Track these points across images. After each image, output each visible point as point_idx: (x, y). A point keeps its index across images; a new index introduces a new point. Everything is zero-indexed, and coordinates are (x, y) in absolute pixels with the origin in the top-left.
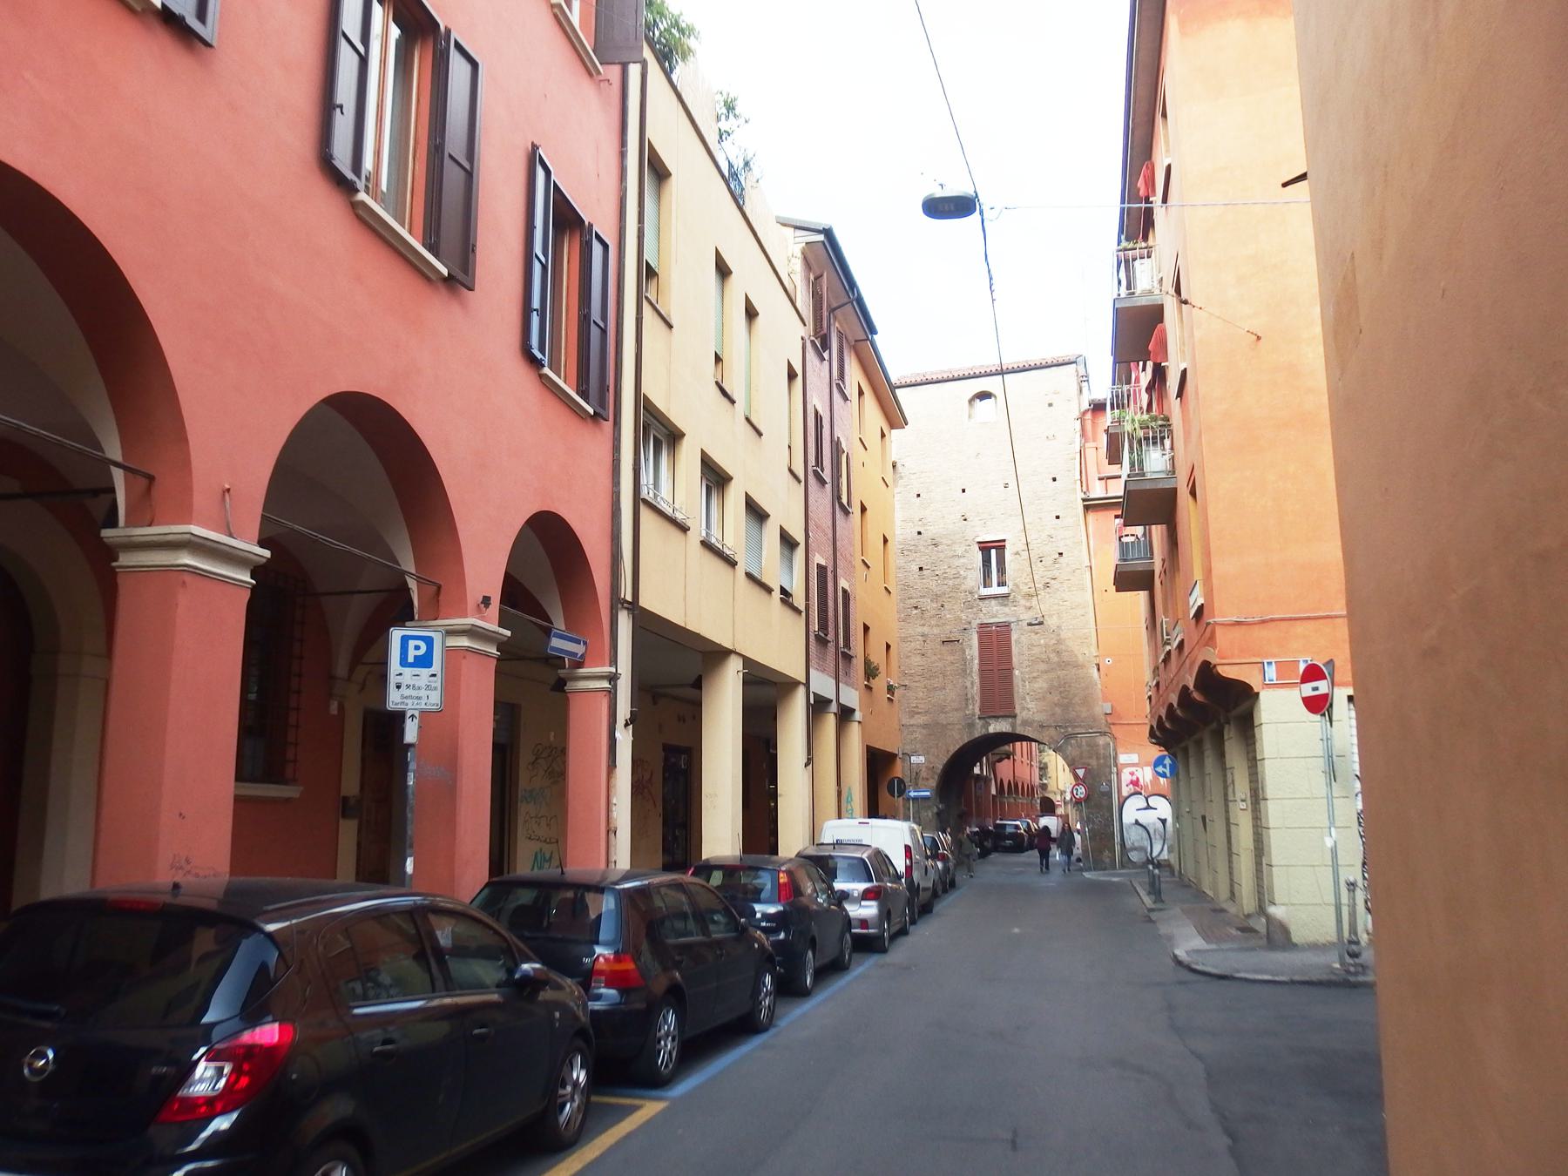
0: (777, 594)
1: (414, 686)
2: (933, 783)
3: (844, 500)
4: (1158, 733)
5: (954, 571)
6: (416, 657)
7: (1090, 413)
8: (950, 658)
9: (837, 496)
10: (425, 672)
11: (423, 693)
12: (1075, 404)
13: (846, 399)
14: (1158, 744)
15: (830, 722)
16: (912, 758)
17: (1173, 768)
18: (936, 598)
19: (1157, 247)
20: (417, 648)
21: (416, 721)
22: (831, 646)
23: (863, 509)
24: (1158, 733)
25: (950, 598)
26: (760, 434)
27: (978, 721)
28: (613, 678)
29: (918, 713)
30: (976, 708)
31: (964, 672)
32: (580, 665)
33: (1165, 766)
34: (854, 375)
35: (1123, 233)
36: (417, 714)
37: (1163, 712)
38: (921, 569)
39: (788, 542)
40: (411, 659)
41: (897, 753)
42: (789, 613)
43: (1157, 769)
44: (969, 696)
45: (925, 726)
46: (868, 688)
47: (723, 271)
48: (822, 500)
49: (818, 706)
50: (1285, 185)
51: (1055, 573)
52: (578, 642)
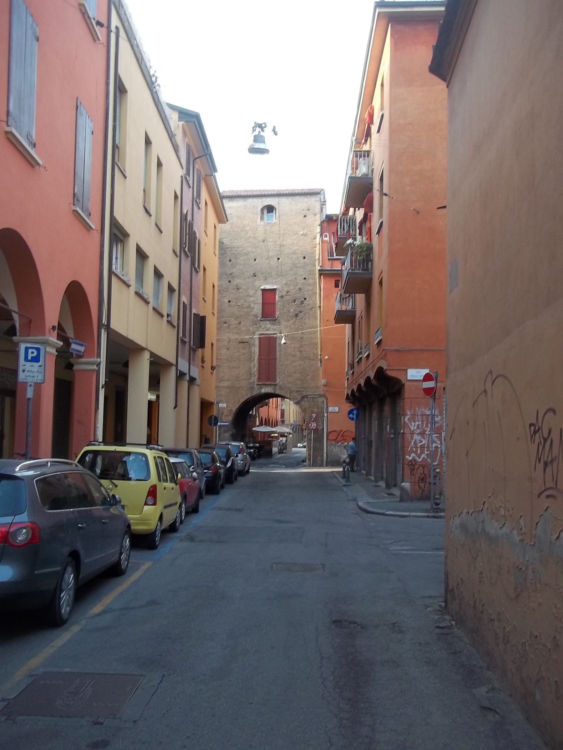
0: (165, 318)
1: (31, 371)
2: (230, 418)
3: (196, 266)
4: (351, 398)
5: (247, 304)
6: (32, 357)
7: (326, 222)
8: (243, 351)
9: (193, 264)
10: (36, 365)
11: (35, 374)
12: (318, 217)
13: (199, 208)
14: (350, 403)
15: (185, 384)
16: (219, 404)
17: (357, 415)
18: (237, 318)
19: (372, 152)
20: (33, 353)
21: (32, 388)
22: (187, 344)
23: (204, 269)
24: (351, 398)
25: (244, 318)
26: (161, 232)
27: (256, 386)
28: (99, 365)
29: (224, 380)
30: (255, 379)
31: (250, 360)
32: (80, 357)
33: (353, 414)
34: (204, 195)
35: (354, 136)
36: (33, 384)
37: (355, 388)
38: (229, 301)
39: (171, 289)
40: (29, 358)
41: (213, 401)
42: (170, 327)
43: (349, 416)
44: (252, 372)
45: (228, 388)
46: (203, 367)
47: (148, 142)
48: (186, 264)
49: (180, 376)
50: (438, 208)
51: (302, 309)
52: (82, 345)
